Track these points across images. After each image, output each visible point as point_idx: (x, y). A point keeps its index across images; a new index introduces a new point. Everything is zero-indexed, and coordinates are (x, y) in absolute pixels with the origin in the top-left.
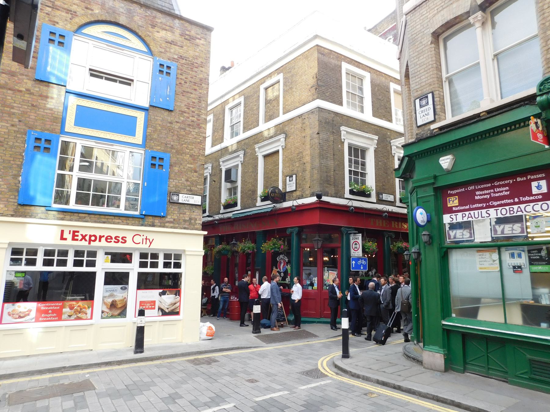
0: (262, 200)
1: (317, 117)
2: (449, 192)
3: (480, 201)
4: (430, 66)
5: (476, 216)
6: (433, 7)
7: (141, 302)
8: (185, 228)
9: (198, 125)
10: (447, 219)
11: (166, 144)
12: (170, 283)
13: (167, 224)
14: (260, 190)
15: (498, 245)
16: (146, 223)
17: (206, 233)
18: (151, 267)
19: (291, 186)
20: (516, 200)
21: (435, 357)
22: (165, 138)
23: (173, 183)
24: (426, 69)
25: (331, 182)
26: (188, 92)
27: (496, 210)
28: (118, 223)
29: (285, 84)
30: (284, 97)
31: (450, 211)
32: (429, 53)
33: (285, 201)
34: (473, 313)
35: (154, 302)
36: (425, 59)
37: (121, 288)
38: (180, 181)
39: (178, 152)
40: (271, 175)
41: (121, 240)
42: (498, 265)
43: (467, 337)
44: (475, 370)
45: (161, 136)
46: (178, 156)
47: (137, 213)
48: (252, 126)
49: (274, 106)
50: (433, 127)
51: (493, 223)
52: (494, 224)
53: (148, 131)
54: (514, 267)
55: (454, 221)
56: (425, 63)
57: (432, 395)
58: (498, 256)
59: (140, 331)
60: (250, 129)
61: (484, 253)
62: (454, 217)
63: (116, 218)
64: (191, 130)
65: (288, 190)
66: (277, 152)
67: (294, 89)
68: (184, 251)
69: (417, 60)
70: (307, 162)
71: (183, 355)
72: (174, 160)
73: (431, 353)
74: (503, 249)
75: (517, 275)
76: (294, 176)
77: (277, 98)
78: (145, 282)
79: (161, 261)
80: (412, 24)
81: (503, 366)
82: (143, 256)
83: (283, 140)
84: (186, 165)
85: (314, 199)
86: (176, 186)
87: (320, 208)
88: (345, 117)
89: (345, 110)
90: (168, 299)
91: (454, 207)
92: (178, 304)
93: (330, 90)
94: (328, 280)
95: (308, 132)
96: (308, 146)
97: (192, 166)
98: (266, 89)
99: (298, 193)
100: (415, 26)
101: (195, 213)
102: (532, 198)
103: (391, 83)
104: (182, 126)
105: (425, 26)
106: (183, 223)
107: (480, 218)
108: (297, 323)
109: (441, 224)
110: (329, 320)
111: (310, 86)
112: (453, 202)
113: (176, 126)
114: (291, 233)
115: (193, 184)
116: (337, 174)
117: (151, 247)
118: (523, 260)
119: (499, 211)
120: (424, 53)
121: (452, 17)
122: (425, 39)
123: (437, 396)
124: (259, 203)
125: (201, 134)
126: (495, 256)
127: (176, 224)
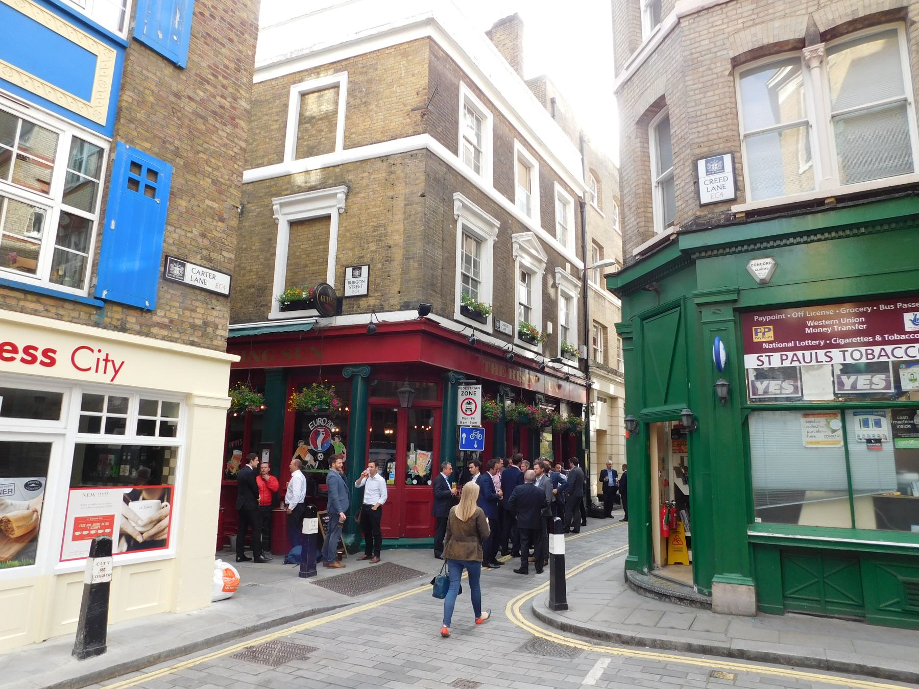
0: (284, 308)
1: (423, 165)
2: (756, 318)
3: (813, 337)
4: (728, 111)
5: (808, 359)
6: (736, 17)
7: (78, 521)
8: (192, 344)
9: (233, 118)
10: (751, 361)
11: (164, 142)
12: (149, 471)
13: (155, 330)
14: (278, 289)
15: (843, 409)
16: (107, 320)
17: (237, 358)
18: (161, 435)
19: (356, 286)
20: (878, 338)
21: (734, 592)
22: (162, 126)
23: (171, 238)
24: (719, 114)
25: (436, 285)
26: (215, 39)
27: (844, 352)
28: (35, 313)
29: (351, 94)
30: (347, 117)
31: (757, 348)
32: (726, 89)
33: (339, 312)
34: (791, 515)
35: (110, 519)
36: (717, 98)
37: (27, 486)
38: (189, 235)
39: (188, 167)
40: (305, 262)
41: (40, 357)
42: (841, 438)
43: (790, 553)
44: (802, 607)
45: (155, 119)
46: (189, 177)
47: (82, 293)
48: (266, 160)
49: (321, 131)
50: (735, 208)
51: (837, 372)
52: (839, 373)
53: (125, 97)
54: (869, 441)
55: (766, 366)
56: (717, 103)
57: (815, 660)
58: (840, 424)
59: (97, 597)
60: (259, 166)
61: (817, 419)
62: (765, 359)
63: (29, 297)
64: (218, 125)
65: (349, 292)
66: (328, 218)
67: (373, 107)
68: (188, 396)
69: (701, 96)
70: (395, 245)
71: (210, 643)
72: (179, 182)
73: (728, 586)
74: (847, 411)
75: (873, 455)
76: (365, 269)
77: (330, 118)
78: (92, 468)
79: (132, 417)
80: (692, 36)
81: (851, 596)
82: (90, 402)
83: (342, 196)
84: (203, 201)
85: (413, 315)
86: (180, 244)
87: (424, 332)
88: (460, 178)
89: (459, 163)
90: (145, 510)
91: (766, 342)
92: (165, 522)
93: (443, 124)
94: (415, 468)
95: (401, 189)
96: (399, 216)
97: (215, 205)
98: (303, 95)
99: (372, 301)
100: (697, 39)
101: (215, 313)
102: (903, 337)
103: (515, 140)
104: (199, 111)
105: (718, 44)
106: (189, 331)
107: (814, 362)
108: (372, 550)
109: (742, 371)
110: (431, 540)
111: (409, 108)
112: (764, 335)
113: (189, 107)
114: (353, 376)
115: (214, 245)
116: (446, 275)
117: (116, 382)
118: (884, 430)
119: (848, 354)
120: (716, 87)
121: (772, 41)
122: (718, 64)
123: (827, 661)
124: (275, 312)
125: (236, 140)
126: (836, 423)
127: (174, 330)
